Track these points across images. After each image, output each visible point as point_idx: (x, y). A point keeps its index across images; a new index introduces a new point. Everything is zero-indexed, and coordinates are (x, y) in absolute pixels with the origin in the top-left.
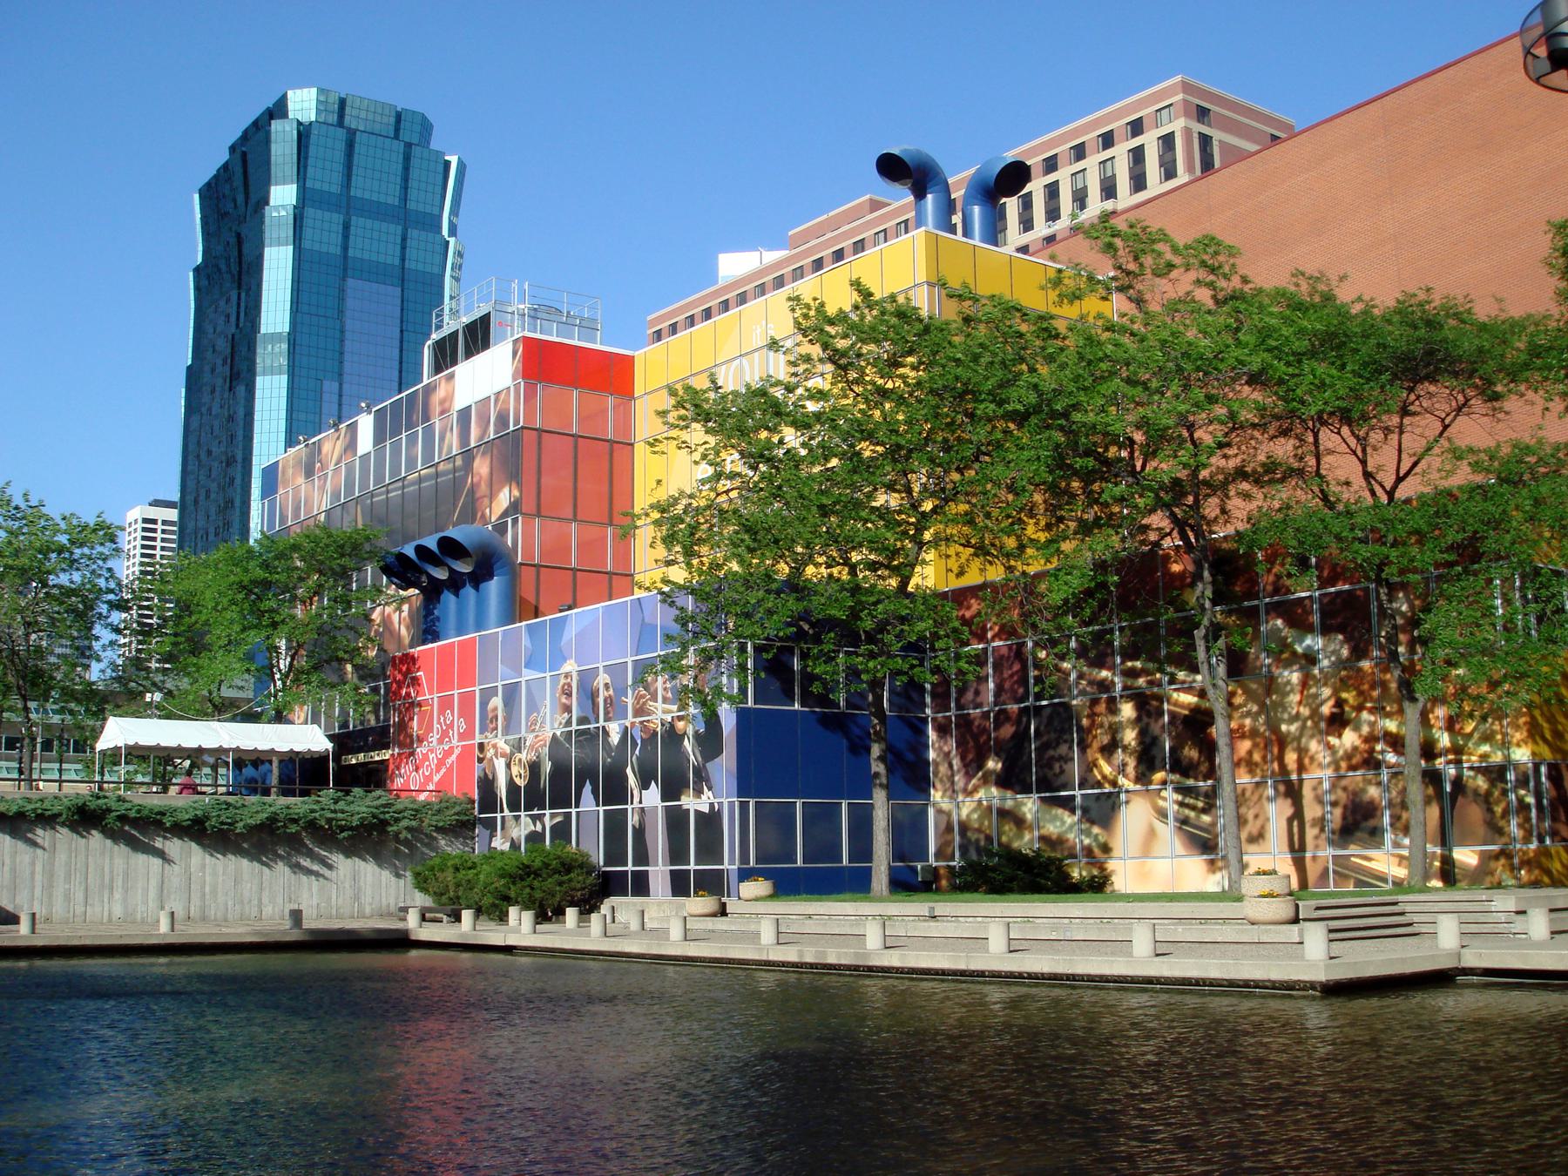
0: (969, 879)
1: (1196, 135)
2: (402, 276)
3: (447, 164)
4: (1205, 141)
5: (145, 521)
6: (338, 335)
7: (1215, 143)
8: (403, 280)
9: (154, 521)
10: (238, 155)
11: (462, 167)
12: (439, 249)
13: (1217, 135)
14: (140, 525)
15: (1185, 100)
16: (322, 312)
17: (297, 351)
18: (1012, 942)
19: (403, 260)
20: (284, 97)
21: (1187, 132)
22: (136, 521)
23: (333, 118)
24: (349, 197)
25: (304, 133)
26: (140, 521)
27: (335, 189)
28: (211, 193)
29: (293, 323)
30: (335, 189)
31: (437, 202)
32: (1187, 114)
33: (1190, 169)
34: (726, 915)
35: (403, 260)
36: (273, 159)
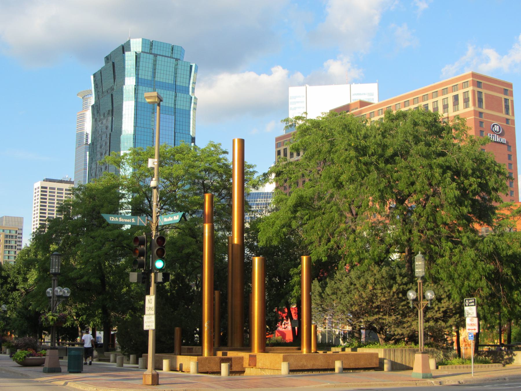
0: (377, 328)
1: (476, 93)
2: (175, 111)
3: (191, 66)
4: (480, 93)
5: (42, 187)
6: (151, 135)
7: (483, 94)
8: (175, 113)
9: (46, 188)
10: (110, 64)
11: (196, 66)
12: (188, 100)
13: (484, 91)
14: (40, 190)
15: (473, 80)
16: (145, 126)
17: (136, 141)
18: (159, 78)
19: (175, 105)
20: (129, 41)
21: (473, 91)
22: (38, 188)
23: (147, 50)
24: (154, 81)
25: (137, 57)
26: (40, 187)
27: (150, 78)
28: (99, 77)
29: (135, 131)
30: (150, 78)
31: (187, 82)
32: (473, 85)
33: (474, 105)
34: (158, 384)
35: (175, 105)
36: (126, 67)
